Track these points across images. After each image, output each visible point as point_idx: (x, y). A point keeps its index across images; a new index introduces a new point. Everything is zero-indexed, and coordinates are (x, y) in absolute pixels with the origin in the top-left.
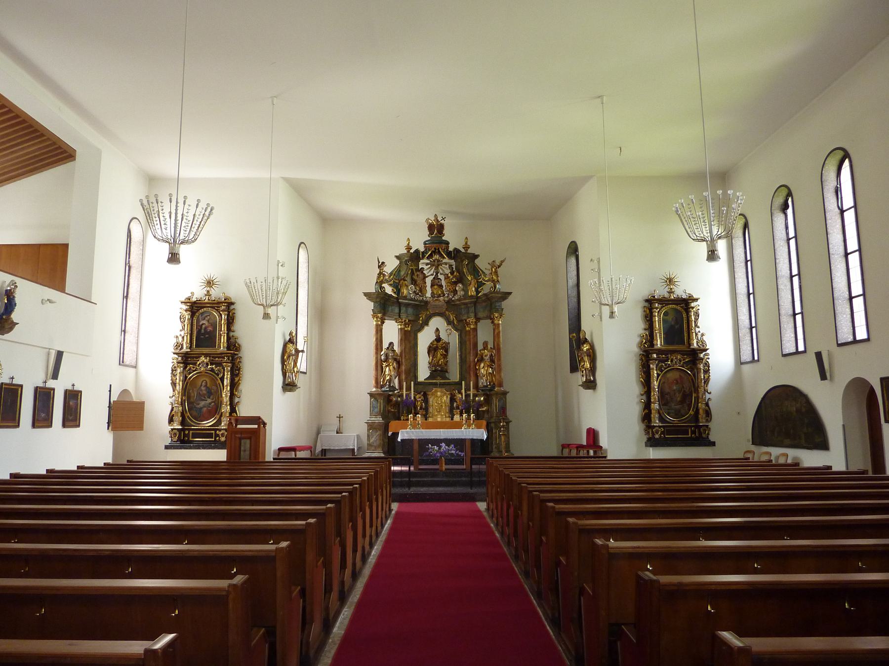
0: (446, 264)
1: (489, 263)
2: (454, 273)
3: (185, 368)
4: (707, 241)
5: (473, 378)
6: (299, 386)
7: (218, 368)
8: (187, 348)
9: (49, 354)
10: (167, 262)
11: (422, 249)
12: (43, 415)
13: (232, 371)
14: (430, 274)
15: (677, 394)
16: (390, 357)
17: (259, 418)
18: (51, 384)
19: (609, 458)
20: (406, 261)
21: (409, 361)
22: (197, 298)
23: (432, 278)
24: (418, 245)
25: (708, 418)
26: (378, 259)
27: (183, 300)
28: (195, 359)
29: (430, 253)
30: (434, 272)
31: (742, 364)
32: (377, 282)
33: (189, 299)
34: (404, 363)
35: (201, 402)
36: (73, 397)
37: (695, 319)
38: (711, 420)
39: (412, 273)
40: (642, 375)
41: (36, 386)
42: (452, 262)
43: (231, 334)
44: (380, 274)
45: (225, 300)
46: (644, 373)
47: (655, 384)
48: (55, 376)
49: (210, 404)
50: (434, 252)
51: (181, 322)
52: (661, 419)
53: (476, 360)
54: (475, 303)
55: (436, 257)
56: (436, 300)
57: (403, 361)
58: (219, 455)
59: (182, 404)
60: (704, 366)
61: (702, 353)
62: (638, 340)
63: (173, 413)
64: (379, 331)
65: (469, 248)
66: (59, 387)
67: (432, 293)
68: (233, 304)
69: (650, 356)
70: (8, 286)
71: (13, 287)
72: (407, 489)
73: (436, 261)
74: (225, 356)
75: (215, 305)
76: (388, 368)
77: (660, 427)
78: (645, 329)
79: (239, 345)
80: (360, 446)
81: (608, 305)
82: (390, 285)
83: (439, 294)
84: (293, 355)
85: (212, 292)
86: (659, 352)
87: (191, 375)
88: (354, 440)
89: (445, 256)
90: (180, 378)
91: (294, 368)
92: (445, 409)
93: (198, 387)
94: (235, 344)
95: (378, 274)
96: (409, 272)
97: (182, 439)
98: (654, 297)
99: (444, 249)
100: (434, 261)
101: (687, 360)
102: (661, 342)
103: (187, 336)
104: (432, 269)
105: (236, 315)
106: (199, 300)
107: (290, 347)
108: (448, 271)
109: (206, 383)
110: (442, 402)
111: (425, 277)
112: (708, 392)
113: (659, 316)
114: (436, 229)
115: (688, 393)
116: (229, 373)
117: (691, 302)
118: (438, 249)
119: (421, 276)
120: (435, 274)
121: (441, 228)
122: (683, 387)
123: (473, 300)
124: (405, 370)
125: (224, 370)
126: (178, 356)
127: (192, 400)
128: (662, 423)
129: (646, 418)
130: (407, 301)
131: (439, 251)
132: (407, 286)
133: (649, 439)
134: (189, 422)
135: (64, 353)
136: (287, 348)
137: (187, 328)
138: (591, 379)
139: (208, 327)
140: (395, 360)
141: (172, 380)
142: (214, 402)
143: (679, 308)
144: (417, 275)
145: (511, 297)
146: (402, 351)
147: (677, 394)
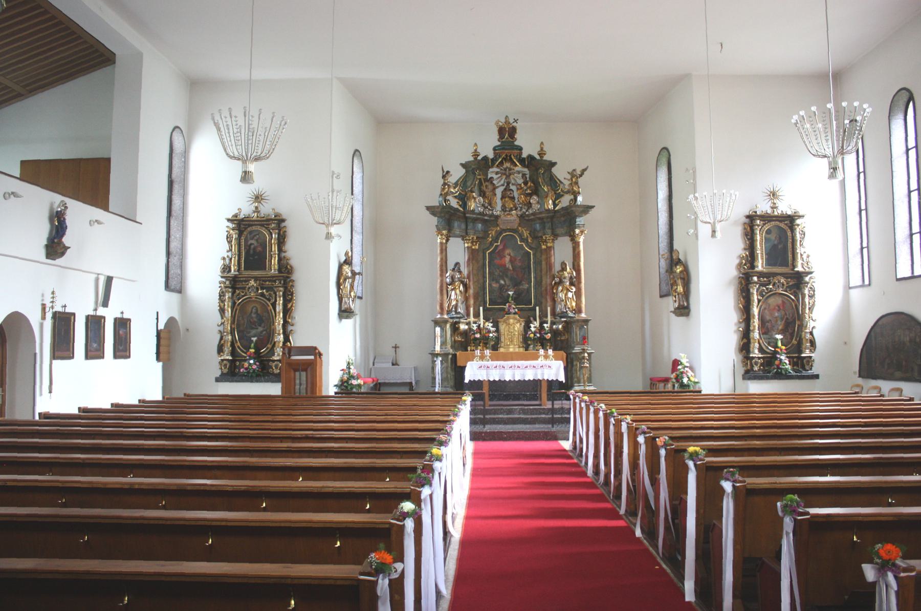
0: (519, 172)
1: (568, 173)
2: (528, 183)
3: (233, 293)
4: (829, 157)
5: (549, 303)
6: (814, 371)
7: (270, 292)
8: (235, 271)
9: (97, 280)
10: (241, 181)
11: (491, 155)
12: (95, 345)
13: (284, 296)
15: (779, 322)
17: (315, 348)
18: (101, 311)
19: (703, 393)
20: (473, 169)
21: (476, 284)
22: (244, 215)
23: (502, 188)
24: (487, 151)
25: (812, 348)
26: (442, 168)
27: (230, 217)
28: (244, 283)
29: (500, 160)
30: (504, 182)
31: (850, 288)
32: (441, 194)
33: (237, 217)
34: (472, 287)
35: (251, 330)
36: (122, 325)
37: (800, 238)
38: (815, 350)
39: (480, 184)
40: (741, 301)
41: (87, 315)
42: (526, 170)
43: (283, 255)
44: (445, 184)
45: (275, 216)
46: (744, 298)
47: (755, 311)
48: (105, 304)
49: (262, 332)
50: (505, 159)
51: (228, 241)
52: (761, 350)
53: (553, 282)
55: (507, 165)
57: (471, 283)
58: (274, 389)
59: (231, 333)
60: (810, 291)
61: (807, 276)
62: (737, 261)
63: (222, 342)
64: (444, 249)
65: (545, 154)
66: (110, 314)
67: (502, 206)
68: (283, 221)
69: (750, 279)
70: (58, 208)
71: (63, 208)
72: (482, 427)
73: (508, 170)
74: (276, 280)
75: (265, 222)
76: (453, 292)
77: (759, 358)
78: (745, 249)
79: (291, 266)
81: (710, 223)
82: (455, 197)
83: (511, 208)
84: (349, 278)
85: (261, 208)
86: (761, 275)
87: (240, 301)
88: (411, 372)
89: (518, 164)
90: (228, 305)
91: (350, 292)
92: (518, 338)
93: (248, 314)
94: (287, 266)
95: (442, 185)
96: (477, 182)
97: (231, 373)
98: (756, 212)
99: (517, 156)
100: (505, 170)
101: (791, 284)
102: (762, 264)
103: (235, 257)
104: (502, 179)
105: (287, 233)
106: (248, 217)
107: (346, 269)
108: (520, 181)
109: (257, 310)
110: (515, 330)
111: (495, 188)
112: (812, 319)
113: (761, 235)
114: (507, 132)
115: (791, 320)
116: (282, 298)
117: (797, 219)
118: (510, 156)
119: (490, 187)
120: (506, 184)
121: (513, 131)
122: (786, 314)
123: (550, 215)
124: (474, 294)
125: (276, 295)
126: (227, 280)
127: (241, 328)
128: (762, 354)
129: (745, 347)
130: (474, 216)
131: (511, 159)
132: (475, 198)
133: (747, 372)
134: (238, 352)
135: (114, 279)
136: (343, 270)
137: (235, 249)
138: (684, 305)
139: (257, 247)
140: (462, 282)
141: (220, 306)
142: (266, 330)
143: (782, 225)
144: (486, 186)
145: (592, 212)
147: (779, 322)
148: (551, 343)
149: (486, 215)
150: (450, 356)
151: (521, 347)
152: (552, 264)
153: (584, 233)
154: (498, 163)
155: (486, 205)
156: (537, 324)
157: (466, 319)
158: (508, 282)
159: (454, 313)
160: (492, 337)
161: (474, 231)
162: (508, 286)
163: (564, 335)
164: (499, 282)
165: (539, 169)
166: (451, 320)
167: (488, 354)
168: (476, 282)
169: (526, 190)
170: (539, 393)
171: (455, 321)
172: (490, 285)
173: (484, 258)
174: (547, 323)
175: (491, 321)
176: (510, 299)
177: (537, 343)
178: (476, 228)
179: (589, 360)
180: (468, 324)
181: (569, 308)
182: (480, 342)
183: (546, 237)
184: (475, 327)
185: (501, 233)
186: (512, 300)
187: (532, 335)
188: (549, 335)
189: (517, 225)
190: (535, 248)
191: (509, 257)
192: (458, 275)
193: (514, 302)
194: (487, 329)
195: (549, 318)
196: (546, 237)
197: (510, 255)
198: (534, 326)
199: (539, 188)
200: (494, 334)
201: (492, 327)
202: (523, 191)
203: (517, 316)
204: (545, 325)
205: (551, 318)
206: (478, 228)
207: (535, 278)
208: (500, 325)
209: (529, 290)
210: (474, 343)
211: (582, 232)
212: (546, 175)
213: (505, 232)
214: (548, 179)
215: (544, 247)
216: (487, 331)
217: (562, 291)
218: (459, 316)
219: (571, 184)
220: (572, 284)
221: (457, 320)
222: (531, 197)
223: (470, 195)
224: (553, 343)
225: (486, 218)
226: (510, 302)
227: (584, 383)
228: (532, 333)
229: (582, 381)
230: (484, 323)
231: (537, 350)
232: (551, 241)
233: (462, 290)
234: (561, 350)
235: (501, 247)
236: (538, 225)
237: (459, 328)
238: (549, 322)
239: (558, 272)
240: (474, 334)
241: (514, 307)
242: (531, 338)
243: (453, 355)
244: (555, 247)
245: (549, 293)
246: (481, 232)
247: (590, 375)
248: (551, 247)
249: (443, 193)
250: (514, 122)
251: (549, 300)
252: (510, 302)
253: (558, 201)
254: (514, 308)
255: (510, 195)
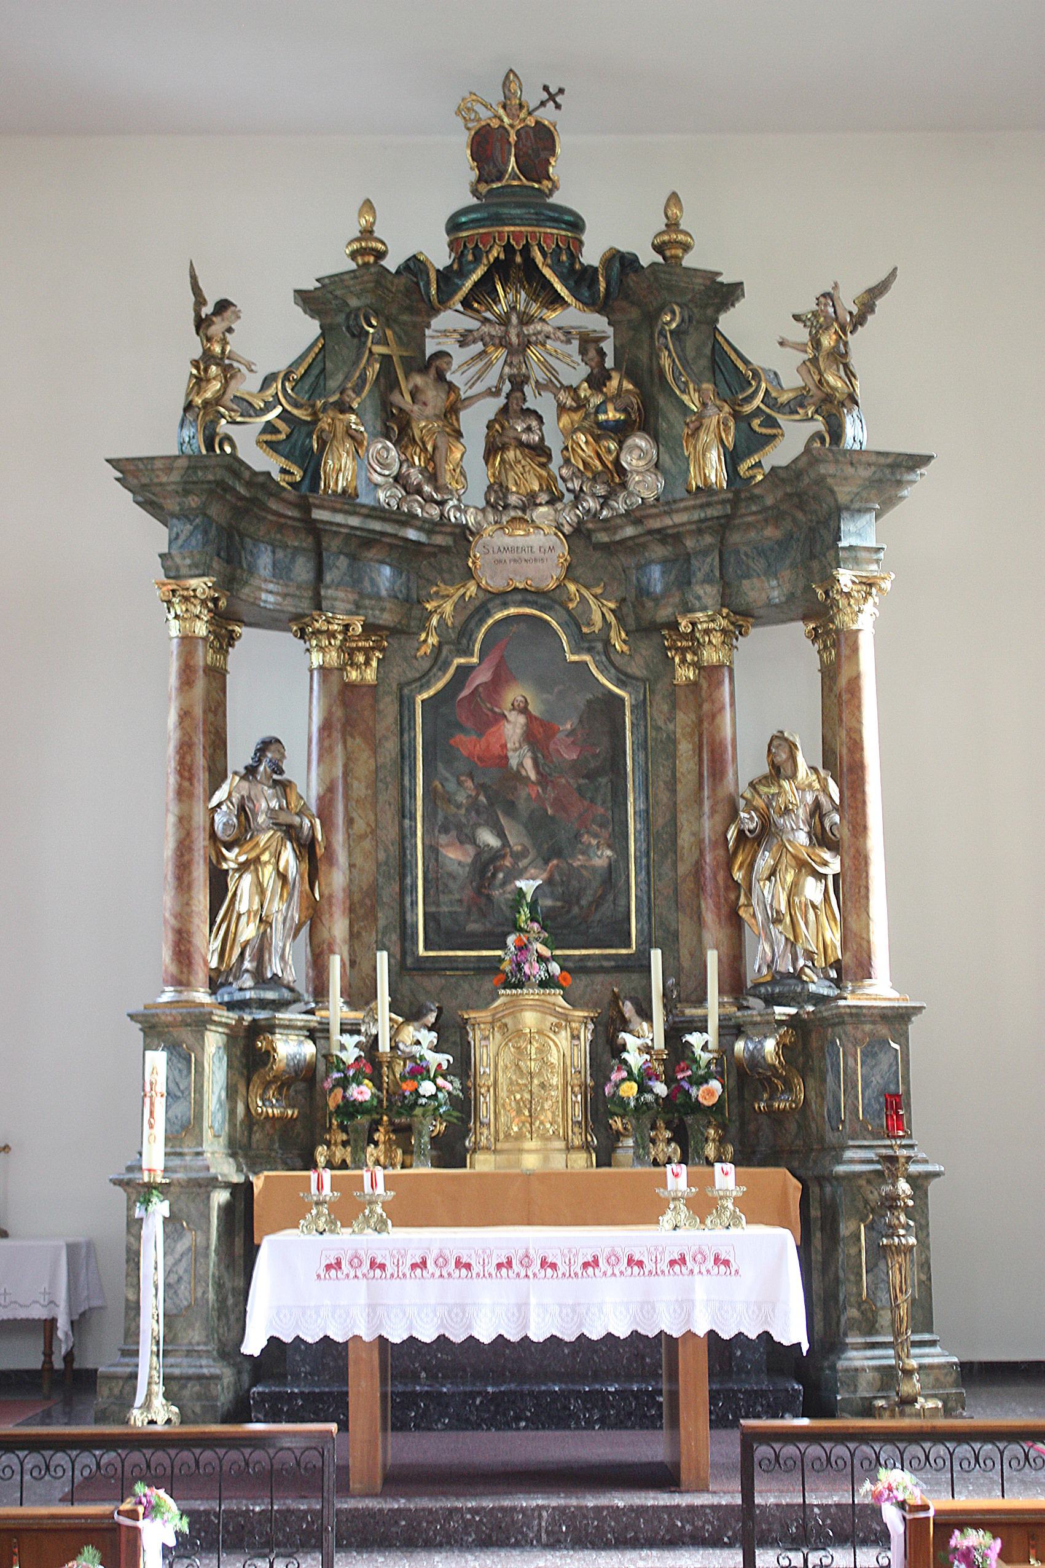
1: (797, 318)
2: (610, 378)
5: (714, 931)
11: (440, 257)
14: (480, 387)
16: (261, 819)
23: (491, 407)
32: (189, 407)
34: (342, 857)
39: (388, 381)
42: (597, 322)
50: (500, 270)
53: (732, 834)
54: (723, 526)
56: (514, 519)
57: (339, 839)
73: (514, 319)
76: (247, 879)
80: (95, 1303)
83: (532, 496)
100: (504, 321)
104: (490, 364)
108: (575, 373)
110: (545, 1062)
118: (526, 250)
120: (507, 387)
123: (711, 512)
124: (349, 892)
130: (354, 521)
140: (290, 832)
144: (414, 394)
146: (330, 789)
148: (722, 1126)
149: (409, 519)
150: (221, 1197)
151: (580, 1148)
152: (722, 745)
153: (881, 589)
154: (469, 284)
155: (416, 477)
156: (655, 1032)
157: (311, 1012)
158: (517, 838)
159: (248, 981)
160: (434, 1097)
161: (352, 597)
162: (517, 856)
163: (789, 1088)
164: (473, 840)
165: (660, 310)
166: (231, 1017)
167: (380, 1189)
168: (362, 837)
169: (599, 409)
170: (664, 1386)
171: (248, 1018)
172: (431, 851)
173: (404, 725)
174: (704, 1029)
175: (431, 1018)
176: (524, 913)
177: (654, 1127)
178: (367, 584)
179: (919, 1212)
180: (317, 1034)
181: (809, 955)
182: (374, 1126)
183: (694, 624)
184: (349, 1050)
185: (482, 611)
186: (533, 920)
187: (629, 1090)
188: (715, 1085)
189: (558, 572)
190: (644, 681)
191: (522, 720)
192: (267, 801)
193: (544, 928)
194: (413, 1058)
195: (713, 1008)
196: (694, 624)
197: (524, 710)
198: (640, 1042)
199: (662, 401)
200: (440, 1081)
201: (437, 1049)
202: (586, 416)
203: (557, 997)
204: (695, 1039)
205: (721, 1005)
206: (373, 582)
207: (645, 816)
208: (475, 1036)
209: (613, 877)
210: (344, 1129)
211: (869, 584)
212: (691, 342)
213: (505, 605)
214: (704, 362)
215: (685, 674)
216: (409, 1065)
217: (773, 873)
218: (270, 995)
219: (814, 361)
220: (822, 838)
221: (262, 1015)
222: (621, 444)
223: (332, 425)
224: (733, 1129)
225: (412, 534)
226: (521, 930)
227: (897, 1334)
228: (631, 1077)
229: (885, 1318)
230: (395, 1031)
231: (655, 1163)
232: (716, 639)
233: (292, 872)
234: (776, 1165)
235: (482, 677)
236: (656, 572)
237: (268, 1056)
238: (713, 1024)
239: (752, 785)
240: (344, 1083)
241: (546, 952)
242: (623, 1102)
243: (234, 1188)
244: (735, 667)
245: (709, 887)
246: (388, 605)
247: (926, 1286)
248: (717, 668)
249: (198, 401)
250: (543, 104)
251: (709, 917)
252: (521, 930)
253: (752, 461)
254: (541, 958)
255: (524, 437)
